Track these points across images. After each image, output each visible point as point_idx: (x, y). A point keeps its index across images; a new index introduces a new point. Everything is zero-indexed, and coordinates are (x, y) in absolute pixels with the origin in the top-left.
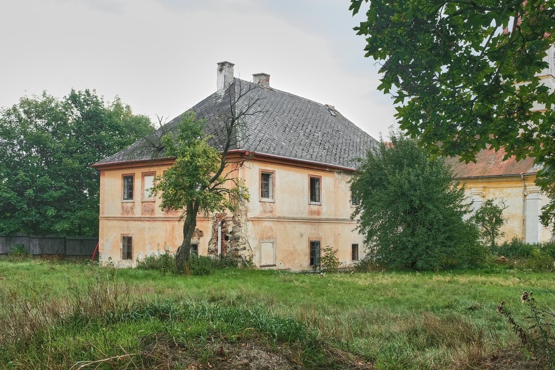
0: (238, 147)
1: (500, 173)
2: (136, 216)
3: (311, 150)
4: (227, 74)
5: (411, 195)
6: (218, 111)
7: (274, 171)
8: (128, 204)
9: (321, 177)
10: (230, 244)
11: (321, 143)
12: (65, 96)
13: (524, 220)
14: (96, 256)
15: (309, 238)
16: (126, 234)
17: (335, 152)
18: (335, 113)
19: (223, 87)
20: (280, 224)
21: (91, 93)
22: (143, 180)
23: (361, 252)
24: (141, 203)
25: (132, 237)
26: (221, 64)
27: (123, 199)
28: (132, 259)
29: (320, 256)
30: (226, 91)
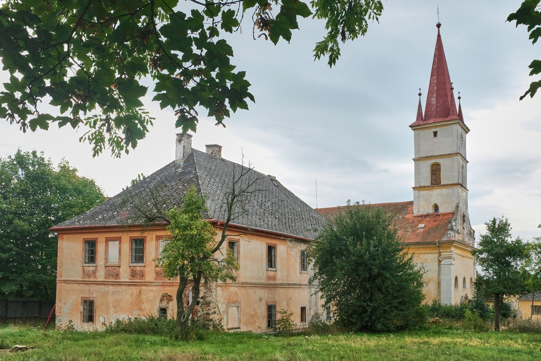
0: (210, 217)
1: (418, 240)
2: (99, 280)
3: (266, 220)
4: (186, 145)
5: (371, 264)
6: (179, 180)
7: (239, 239)
8: (90, 268)
9: (276, 244)
10: (202, 308)
11: (272, 213)
12: (10, 156)
13: (439, 283)
14: (53, 318)
15: (266, 302)
16: (88, 298)
17: (284, 221)
18: (277, 184)
19: (182, 157)
20: (243, 289)
21: (39, 155)
22: (107, 245)
23: (308, 314)
24: (105, 268)
25: (94, 300)
26: (180, 135)
27: (83, 263)
28: (93, 322)
29: (275, 318)
30: (184, 161)
